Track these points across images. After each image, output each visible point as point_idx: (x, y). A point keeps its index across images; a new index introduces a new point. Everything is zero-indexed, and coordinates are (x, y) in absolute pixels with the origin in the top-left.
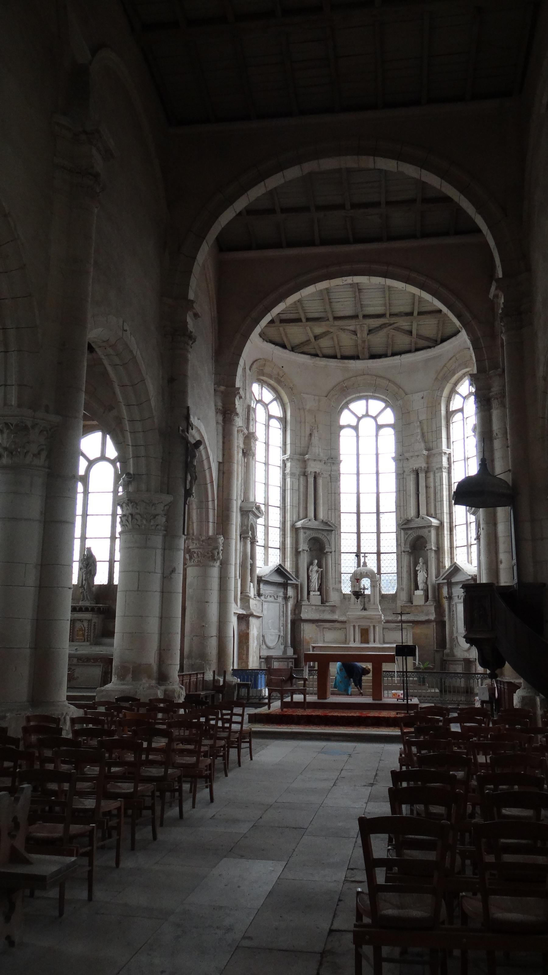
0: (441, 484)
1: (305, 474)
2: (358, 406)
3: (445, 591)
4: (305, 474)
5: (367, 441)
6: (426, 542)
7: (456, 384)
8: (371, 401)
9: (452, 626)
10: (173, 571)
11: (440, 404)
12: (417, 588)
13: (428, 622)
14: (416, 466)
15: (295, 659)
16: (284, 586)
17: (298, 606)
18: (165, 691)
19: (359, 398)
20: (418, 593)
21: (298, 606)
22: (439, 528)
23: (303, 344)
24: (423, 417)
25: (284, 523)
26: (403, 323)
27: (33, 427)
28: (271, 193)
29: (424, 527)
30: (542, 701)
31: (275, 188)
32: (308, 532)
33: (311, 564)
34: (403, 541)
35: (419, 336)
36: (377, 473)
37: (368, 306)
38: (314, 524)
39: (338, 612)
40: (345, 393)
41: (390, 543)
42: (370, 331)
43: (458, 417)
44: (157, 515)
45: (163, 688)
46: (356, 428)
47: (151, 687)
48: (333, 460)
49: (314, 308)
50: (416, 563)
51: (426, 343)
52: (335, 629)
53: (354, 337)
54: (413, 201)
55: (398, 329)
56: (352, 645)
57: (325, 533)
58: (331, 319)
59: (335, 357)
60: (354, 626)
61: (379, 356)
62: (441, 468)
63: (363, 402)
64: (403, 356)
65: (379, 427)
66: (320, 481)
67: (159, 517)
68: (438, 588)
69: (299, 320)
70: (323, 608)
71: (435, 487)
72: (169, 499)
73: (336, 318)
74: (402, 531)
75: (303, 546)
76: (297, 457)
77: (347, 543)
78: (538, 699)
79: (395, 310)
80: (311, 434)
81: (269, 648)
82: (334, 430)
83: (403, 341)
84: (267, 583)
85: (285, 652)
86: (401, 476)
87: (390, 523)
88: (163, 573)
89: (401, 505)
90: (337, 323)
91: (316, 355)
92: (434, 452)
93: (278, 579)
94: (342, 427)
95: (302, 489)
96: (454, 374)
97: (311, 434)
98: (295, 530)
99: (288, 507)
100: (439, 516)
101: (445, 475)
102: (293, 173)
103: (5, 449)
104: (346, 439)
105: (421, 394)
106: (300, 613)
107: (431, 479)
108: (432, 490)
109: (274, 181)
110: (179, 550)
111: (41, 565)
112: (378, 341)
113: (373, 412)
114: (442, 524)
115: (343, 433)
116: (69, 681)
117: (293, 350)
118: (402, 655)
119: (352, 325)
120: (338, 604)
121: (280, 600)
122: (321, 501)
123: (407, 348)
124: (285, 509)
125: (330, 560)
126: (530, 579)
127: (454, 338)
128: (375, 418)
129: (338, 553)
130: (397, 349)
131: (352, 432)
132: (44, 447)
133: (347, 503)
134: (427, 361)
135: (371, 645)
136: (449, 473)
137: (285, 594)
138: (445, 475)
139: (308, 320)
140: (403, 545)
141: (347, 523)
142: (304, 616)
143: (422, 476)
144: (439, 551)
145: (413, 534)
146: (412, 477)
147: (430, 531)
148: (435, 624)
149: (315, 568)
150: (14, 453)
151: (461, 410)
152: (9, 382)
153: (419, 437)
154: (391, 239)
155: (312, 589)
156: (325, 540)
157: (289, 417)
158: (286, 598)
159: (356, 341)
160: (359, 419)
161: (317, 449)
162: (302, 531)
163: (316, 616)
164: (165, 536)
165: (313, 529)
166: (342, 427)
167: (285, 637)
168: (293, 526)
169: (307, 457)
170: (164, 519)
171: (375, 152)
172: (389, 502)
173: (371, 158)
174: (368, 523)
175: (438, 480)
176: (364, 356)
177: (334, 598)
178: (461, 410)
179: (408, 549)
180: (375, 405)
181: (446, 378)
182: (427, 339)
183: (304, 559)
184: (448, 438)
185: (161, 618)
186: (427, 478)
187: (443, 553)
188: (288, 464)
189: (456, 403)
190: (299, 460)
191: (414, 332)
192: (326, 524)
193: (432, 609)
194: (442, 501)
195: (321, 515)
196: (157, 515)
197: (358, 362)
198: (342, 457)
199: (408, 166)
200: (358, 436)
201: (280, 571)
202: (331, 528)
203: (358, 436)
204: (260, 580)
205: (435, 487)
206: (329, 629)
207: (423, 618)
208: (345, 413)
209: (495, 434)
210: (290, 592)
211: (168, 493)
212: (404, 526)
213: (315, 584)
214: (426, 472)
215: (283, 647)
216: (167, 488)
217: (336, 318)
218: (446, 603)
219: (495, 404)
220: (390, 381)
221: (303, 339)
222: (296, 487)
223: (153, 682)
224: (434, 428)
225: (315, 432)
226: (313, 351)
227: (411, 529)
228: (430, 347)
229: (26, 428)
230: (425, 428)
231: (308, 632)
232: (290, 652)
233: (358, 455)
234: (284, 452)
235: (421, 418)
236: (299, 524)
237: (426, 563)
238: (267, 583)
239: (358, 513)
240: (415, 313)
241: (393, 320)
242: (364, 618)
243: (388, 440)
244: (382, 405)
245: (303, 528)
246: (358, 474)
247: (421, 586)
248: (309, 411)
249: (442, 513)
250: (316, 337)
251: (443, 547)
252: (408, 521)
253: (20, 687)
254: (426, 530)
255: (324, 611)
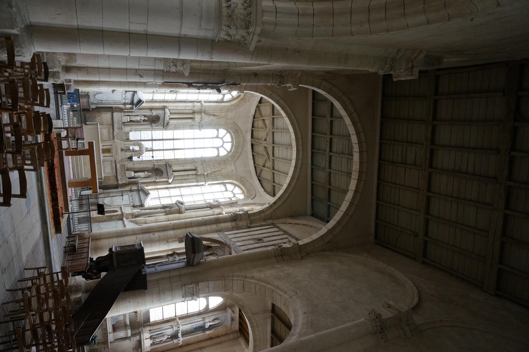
0: (190, 182)
1: (194, 113)
2: (228, 138)
3: (134, 188)
4: (194, 113)
5: (210, 142)
6: (160, 176)
7: (239, 187)
8: (230, 144)
9: (116, 192)
10: (141, 76)
11: (230, 179)
12: (135, 172)
13: (117, 180)
14: (199, 169)
15: (89, 109)
16: (132, 103)
17: (121, 110)
18: (58, 72)
19: (232, 138)
20: (133, 173)
21: (121, 110)
22: (167, 183)
23: (260, 112)
24: (223, 171)
25: (167, 102)
26: (269, 164)
27: (248, 33)
28: (341, 117)
29: (168, 175)
30: (80, 298)
31: (344, 121)
32: (163, 115)
33: (145, 116)
34: (160, 163)
35: (262, 170)
36: (194, 148)
37: (279, 150)
38: (167, 118)
39: (118, 131)
40: (235, 131)
41: (159, 156)
42: (265, 147)
43: (222, 188)
44: (176, 67)
45: (60, 70)
46: (217, 137)
47: (59, 62)
48: (201, 126)
49: (279, 123)
50: (148, 171)
51: (258, 173)
52: (109, 135)
53: (263, 139)
54: (330, 184)
55: (266, 161)
56: (101, 145)
57: (162, 124)
58: (273, 130)
59: (253, 127)
60: (111, 145)
61: (252, 148)
62: (198, 182)
63: (230, 140)
64: (252, 160)
65: (218, 148)
66: (190, 121)
67: (175, 68)
68: (136, 183)
69: (273, 114)
70: (120, 123)
71: (188, 179)
72: (187, 74)
73: (273, 133)
74: (165, 163)
75: (155, 113)
76: (203, 109)
77: (158, 134)
78: (79, 295)
79: (276, 162)
80: (214, 115)
81: (95, 95)
82: (217, 126)
83: (260, 161)
84: (133, 96)
85: (93, 104)
86: (193, 161)
87: (169, 156)
88: (139, 70)
89: (178, 161)
90: (271, 134)
91: (254, 118)
92: (206, 178)
93: (135, 101)
94: (218, 130)
95: (186, 111)
96: (243, 186)
97: (214, 115)
98: (164, 108)
99: (176, 104)
100: (174, 182)
101: (195, 184)
102: (351, 130)
103: (233, 11)
104: (212, 132)
105: (234, 170)
106: (117, 111)
107: (192, 177)
108: (187, 178)
109: (347, 120)
110: (155, 79)
111: (146, 34)
112: (260, 149)
113: (225, 145)
114: (170, 184)
115: (215, 131)
116: (52, 53)
117: (257, 106)
118: (98, 208)
119: (270, 139)
120: (123, 130)
121: (124, 101)
122: (179, 121)
123: (257, 163)
124: (176, 102)
125: (149, 127)
126: (148, 278)
127: (260, 186)
128: (222, 146)
129: (152, 129)
130: (256, 158)
131: (215, 135)
132: (233, 39)
133: (178, 133)
134: (250, 172)
135: (102, 155)
136: (196, 186)
137: (127, 104)
138: (195, 184)
139: (273, 118)
140: (157, 164)
141: (167, 134)
142: (115, 114)
143: (194, 172)
144: (155, 183)
145: (163, 169)
146: (193, 168)
147: (165, 178)
148: (116, 183)
149: (143, 119)
150: (230, 19)
151: (226, 190)
152: (278, 15)
153: (213, 170)
154: (312, 169)
155: (131, 117)
156: (158, 124)
157: (223, 104)
158: (125, 104)
159: (261, 140)
160: (222, 139)
161: (206, 118)
162: (163, 112)
163: (115, 120)
164: (163, 71)
165: (164, 116)
166: (218, 130)
167: (101, 104)
168: (166, 107)
169: (203, 114)
170: (174, 70)
171: (359, 180)
172: (180, 155)
173: (357, 178)
174: (168, 145)
175: (192, 180)
176: (256, 147)
177: (126, 129)
178: (226, 190)
179: (156, 167)
180: (228, 146)
181: (242, 182)
182: (260, 173)
183: (148, 113)
184: (213, 184)
185: (109, 68)
186: (193, 174)
187: (155, 185)
188: (199, 104)
189: (230, 187)
190: (201, 109)
191: (264, 168)
192: (168, 124)
193: (124, 182)
194: (182, 183)
195: (172, 122)
196: (176, 67)
197: (250, 137)
198: (202, 130)
199: (352, 196)
200: (213, 138)
201: (140, 102)
202: (165, 126)
203: (213, 138)
204: (135, 92)
205: (188, 179)
206: (109, 131)
207: (119, 177)
208: (225, 131)
209: (219, 225)
210: (128, 106)
211: (190, 73)
212: (168, 164)
213: (134, 119)
214: (196, 174)
215: (96, 102)
216: (193, 72)
217: (273, 133)
218: (128, 188)
219: (234, 224)
220: (241, 154)
221: (263, 113)
222: (187, 108)
223: (63, 63)
224: (217, 177)
225: (216, 118)
226: (256, 116)
227: (167, 168)
228: (256, 173)
229: (247, 28)
230: (218, 173)
231: (106, 116)
232: (93, 107)
233: (204, 138)
234: (205, 102)
235: (222, 170)
236: (167, 111)
237: (149, 177)
238: (133, 96)
239: (173, 139)
240: (273, 171)
241: (271, 160)
242: (117, 151)
243: (211, 153)
244: (229, 150)
245: (165, 113)
246: (194, 139)
247: (136, 174)
248: (227, 114)
249: (175, 184)
250: (263, 120)
251: (158, 185)
252: (171, 167)
253: (42, 17)
254: (166, 176)
255: (119, 124)
